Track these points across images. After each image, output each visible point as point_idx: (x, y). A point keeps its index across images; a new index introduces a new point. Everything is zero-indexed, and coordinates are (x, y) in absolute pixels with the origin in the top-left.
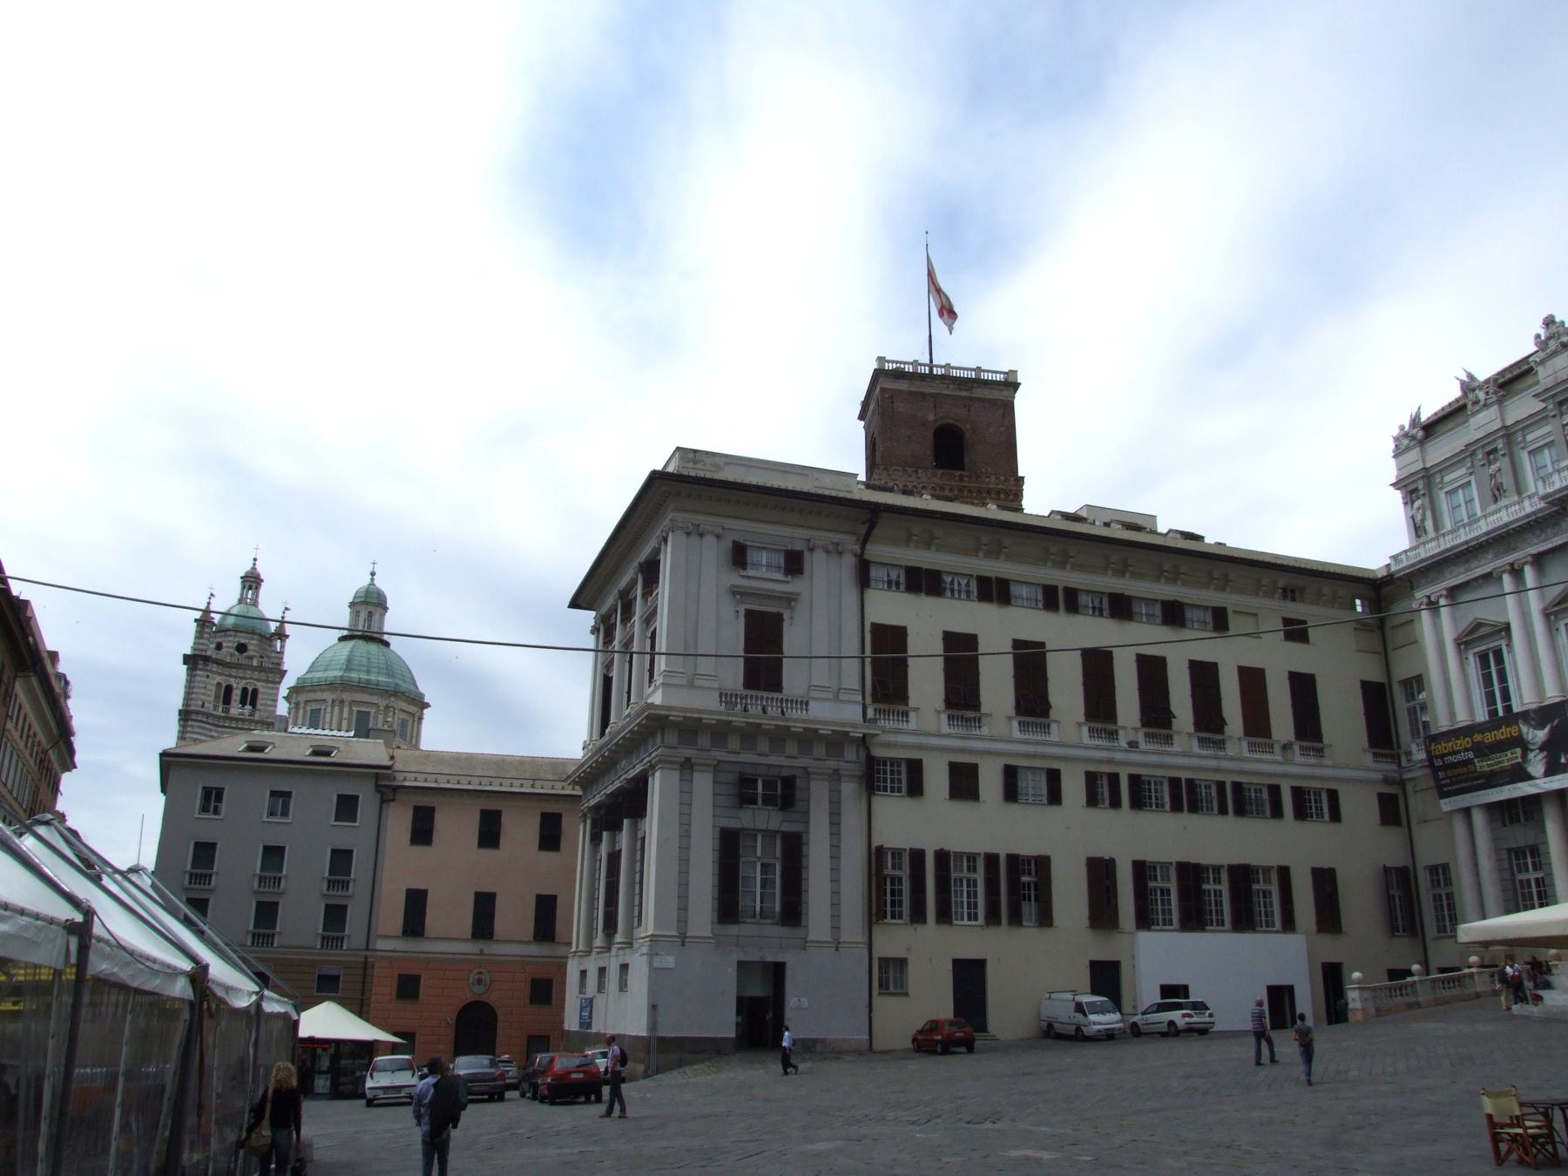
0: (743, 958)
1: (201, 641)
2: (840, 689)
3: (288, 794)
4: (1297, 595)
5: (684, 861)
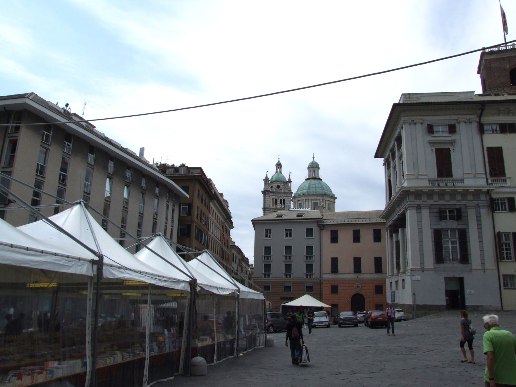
0: (446, 276)
1: (266, 186)
2: (476, 174)
3: (291, 230)
5: (421, 242)
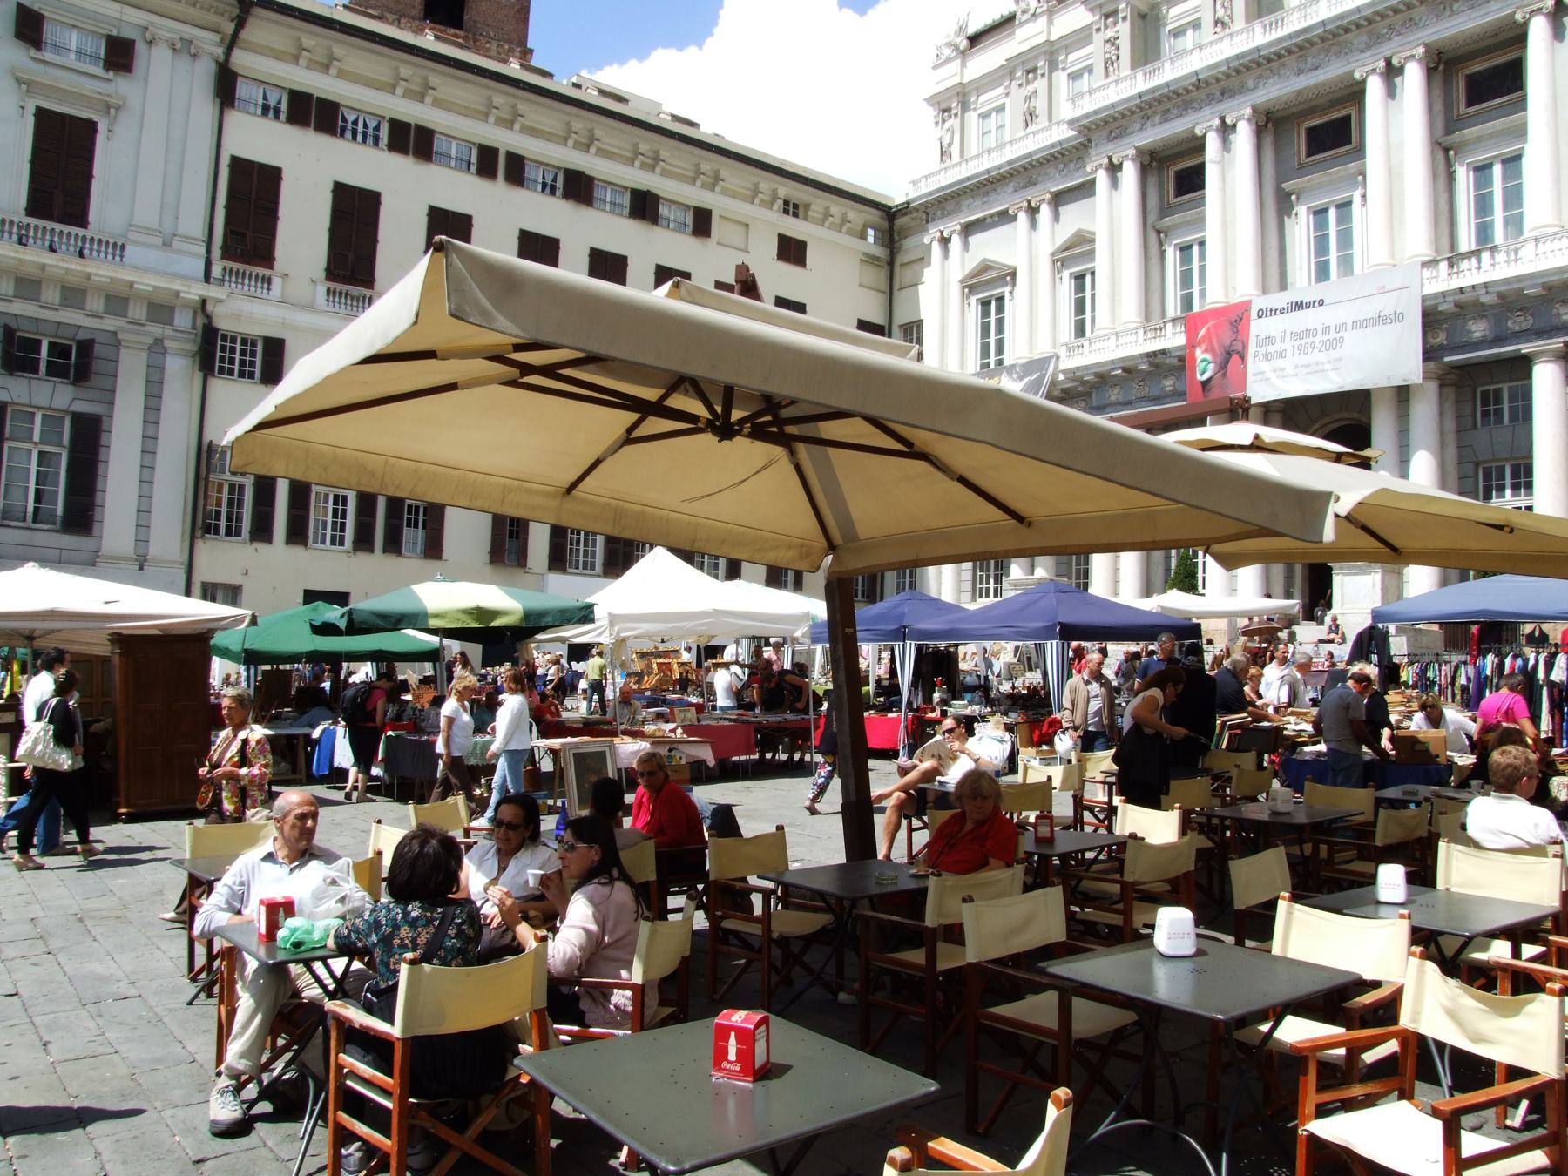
2: (175, 235)
4: (801, 211)
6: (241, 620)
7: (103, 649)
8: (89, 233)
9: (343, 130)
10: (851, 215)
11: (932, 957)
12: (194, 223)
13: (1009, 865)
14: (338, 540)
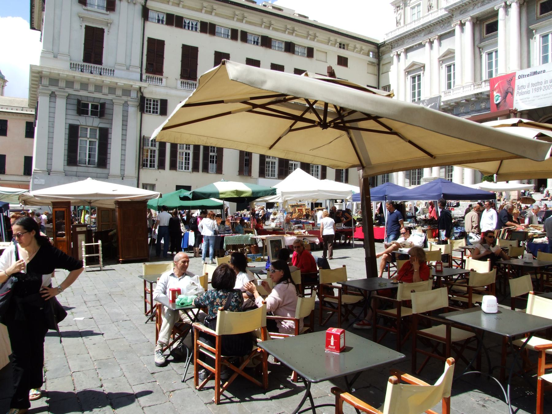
4: (346, 47)
6: (157, 196)
7: (113, 206)
8: (102, 67)
9: (185, 26)
10: (364, 47)
11: (399, 312)
12: (136, 61)
13: (427, 280)
14: (187, 168)
